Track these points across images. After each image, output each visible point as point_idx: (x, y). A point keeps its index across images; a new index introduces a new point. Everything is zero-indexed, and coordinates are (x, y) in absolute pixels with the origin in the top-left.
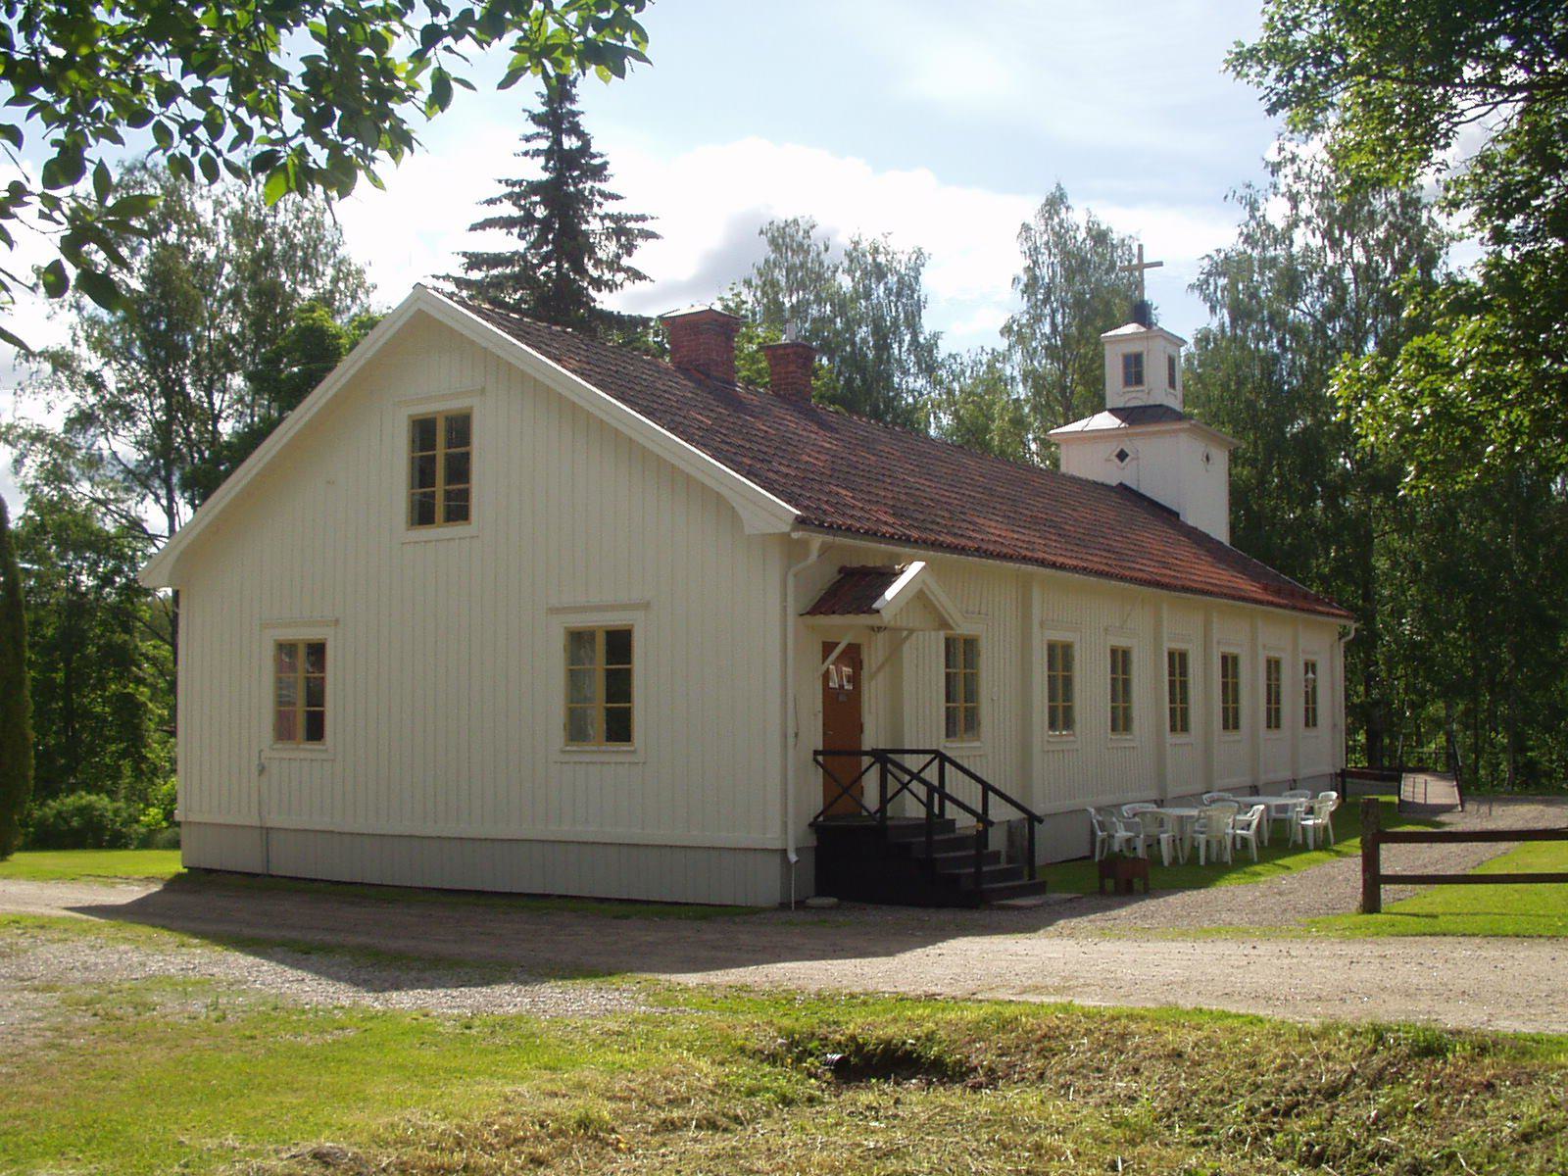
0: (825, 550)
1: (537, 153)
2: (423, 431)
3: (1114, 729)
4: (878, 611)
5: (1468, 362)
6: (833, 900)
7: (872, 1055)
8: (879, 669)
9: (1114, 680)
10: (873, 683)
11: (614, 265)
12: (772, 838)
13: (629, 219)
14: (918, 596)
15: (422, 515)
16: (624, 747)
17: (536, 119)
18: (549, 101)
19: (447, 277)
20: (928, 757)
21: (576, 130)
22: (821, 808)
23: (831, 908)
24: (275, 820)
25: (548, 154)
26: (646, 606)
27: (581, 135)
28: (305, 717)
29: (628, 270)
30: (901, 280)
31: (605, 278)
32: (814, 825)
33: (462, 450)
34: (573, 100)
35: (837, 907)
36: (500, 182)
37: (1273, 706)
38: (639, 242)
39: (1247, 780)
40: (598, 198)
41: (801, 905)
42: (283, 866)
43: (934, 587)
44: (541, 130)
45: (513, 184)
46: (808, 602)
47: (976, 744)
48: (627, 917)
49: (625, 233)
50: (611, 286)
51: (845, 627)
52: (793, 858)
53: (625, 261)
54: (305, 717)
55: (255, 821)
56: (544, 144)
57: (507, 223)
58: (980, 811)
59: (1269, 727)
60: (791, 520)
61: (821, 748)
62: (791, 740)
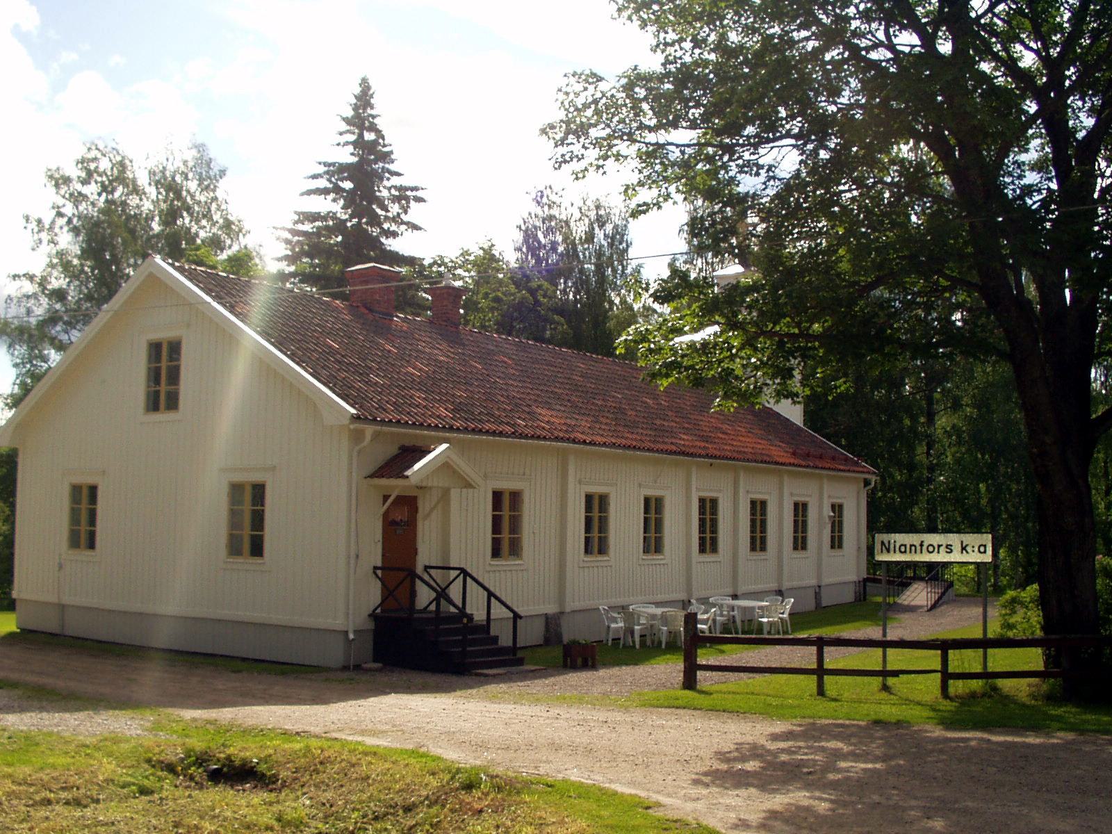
0: (376, 436)
1: (347, 143)
2: (155, 348)
3: (587, 551)
4: (407, 477)
5: (743, 329)
6: (380, 665)
7: (234, 768)
8: (432, 510)
9: (646, 520)
10: (427, 522)
11: (396, 219)
12: (338, 623)
13: (407, 189)
14: (444, 466)
15: (153, 404)
16: (258, 560)
17: (347, 121)
18: (356, 108)
19: (283, 229)
20: (458, 572)
21: (373, 128)
22: (378, 600)
23: (376, 670)
24: (67, 599)
25: (355, 144)
26: (274, 468)
27: (379, 133)
28: (84, 533)
29: (407, 224)
30: (616, 227)
31: (391, 229)
32: (373, 615)
33: (175, 363)
34: (372, 108)
35: (380, 670)
36: (320, 163)
37: (800, 535)
38: (412, 203)
39: (773, 586)
40: (387, 175)
41: (357, 667)
42: (75, 627)
43: (454, 457)
44: (348, 128)
45: (330, 165)
46: (371, 468)
47: (520, 562)
48: (239, 671)
49: (404, 196)
50: (394, 234)
51: (395, 486)
52: (351, 636)
53: (405, 218)
54: (84, 533)
55: (56, 601)
56: (352, 138)
57: (325, 192)
58: (461, 606)
59: (832, 547)
60: (349, 416)
61: (379, 564)
62: (353, 561)
